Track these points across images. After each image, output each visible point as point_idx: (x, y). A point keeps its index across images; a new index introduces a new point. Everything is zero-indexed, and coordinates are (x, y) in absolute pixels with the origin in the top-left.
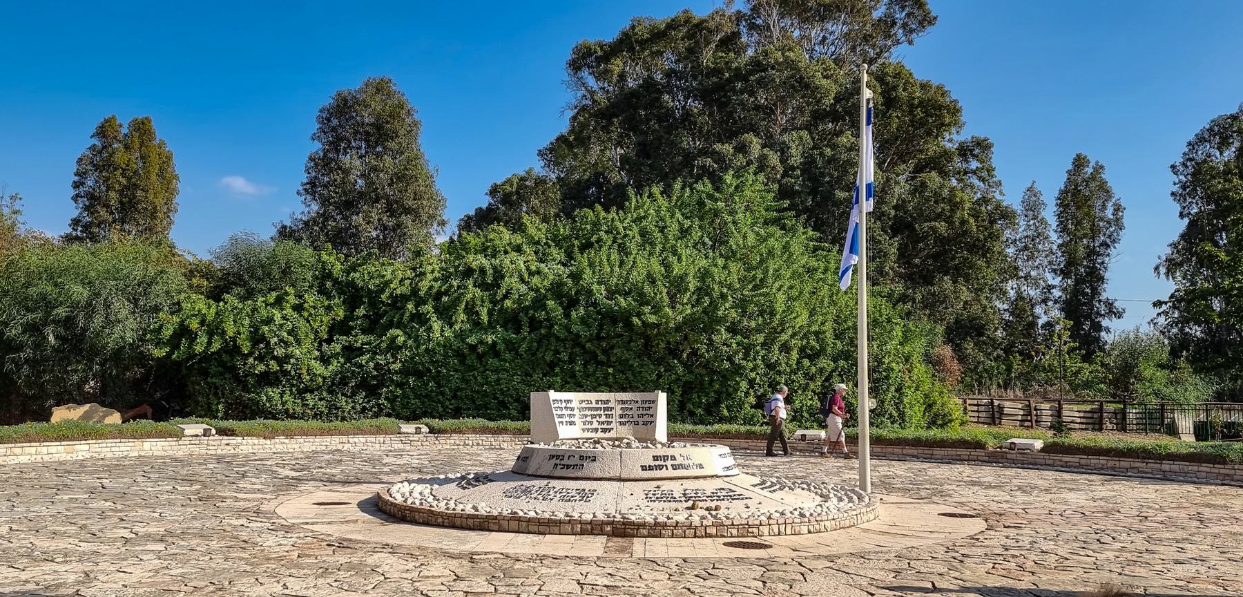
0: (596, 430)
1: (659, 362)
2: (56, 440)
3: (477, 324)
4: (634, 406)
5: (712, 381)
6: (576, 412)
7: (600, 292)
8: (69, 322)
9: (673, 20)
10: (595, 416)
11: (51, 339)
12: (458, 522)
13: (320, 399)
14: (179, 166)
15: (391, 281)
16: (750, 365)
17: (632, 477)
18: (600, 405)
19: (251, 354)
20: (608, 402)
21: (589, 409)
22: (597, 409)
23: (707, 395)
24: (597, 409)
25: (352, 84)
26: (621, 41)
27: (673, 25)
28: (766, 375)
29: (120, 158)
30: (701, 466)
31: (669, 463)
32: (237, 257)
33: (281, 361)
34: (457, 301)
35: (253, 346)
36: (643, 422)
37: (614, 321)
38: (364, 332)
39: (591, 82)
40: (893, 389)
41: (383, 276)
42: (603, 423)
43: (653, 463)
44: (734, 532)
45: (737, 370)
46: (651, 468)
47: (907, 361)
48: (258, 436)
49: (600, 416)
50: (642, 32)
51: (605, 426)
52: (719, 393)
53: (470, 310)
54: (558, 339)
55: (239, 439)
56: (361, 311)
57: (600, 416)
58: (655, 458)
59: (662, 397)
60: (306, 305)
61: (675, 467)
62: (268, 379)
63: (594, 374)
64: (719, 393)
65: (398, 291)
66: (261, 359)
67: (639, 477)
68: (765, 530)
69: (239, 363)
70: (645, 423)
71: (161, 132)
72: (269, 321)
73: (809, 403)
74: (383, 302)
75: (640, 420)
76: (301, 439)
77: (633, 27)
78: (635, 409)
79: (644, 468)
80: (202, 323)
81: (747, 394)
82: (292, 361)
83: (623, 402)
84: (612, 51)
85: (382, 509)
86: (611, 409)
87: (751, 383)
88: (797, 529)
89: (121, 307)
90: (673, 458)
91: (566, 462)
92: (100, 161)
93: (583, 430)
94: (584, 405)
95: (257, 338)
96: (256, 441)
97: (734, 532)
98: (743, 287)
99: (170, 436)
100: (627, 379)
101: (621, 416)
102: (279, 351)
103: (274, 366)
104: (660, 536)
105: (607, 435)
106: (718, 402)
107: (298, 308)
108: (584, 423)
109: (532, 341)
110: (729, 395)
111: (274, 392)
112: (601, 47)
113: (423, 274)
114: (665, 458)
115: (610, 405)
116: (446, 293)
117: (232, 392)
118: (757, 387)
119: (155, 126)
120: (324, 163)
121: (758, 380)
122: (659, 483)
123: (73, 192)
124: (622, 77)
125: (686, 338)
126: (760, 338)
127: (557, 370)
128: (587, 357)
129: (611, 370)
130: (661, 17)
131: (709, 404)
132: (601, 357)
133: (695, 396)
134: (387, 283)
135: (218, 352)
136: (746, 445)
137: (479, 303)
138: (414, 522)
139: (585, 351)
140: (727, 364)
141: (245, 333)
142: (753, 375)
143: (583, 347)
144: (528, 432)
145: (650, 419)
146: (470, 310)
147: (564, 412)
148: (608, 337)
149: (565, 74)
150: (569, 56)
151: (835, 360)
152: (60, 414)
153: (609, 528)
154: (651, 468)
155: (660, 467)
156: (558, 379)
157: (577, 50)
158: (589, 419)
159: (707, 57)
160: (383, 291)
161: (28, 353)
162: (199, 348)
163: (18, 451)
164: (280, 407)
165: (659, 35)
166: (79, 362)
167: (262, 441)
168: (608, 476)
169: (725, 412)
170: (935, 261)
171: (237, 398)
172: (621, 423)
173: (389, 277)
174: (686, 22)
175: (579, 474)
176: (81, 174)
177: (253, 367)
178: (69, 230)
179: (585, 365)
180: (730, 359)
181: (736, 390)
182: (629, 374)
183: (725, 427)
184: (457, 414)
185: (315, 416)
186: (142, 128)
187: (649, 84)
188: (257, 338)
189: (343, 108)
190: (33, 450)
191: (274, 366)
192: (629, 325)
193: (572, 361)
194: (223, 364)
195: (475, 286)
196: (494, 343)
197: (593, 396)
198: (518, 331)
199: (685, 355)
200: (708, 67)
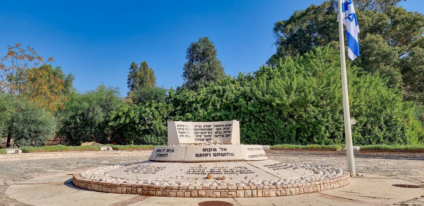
0: (203, 140)
1: (285, 120)
3: (216, 110)
4: (222, 128)
5: (309, 127)
7: (259, 94)
8: (83, 114)
9: (308, 9)
10: (203, 133)
11: (78, 120)
12: (76, 184)
13: (163, 139)
14: (156, 75)
15: (189, 97)
16: (326, 120)
17: (190, 160)
18: (206, 128)
19: (139, 123)
20: (210, 126)
21: (200, 129)
22: (204, 130)
23: (307, 133)
24: (204, 130)
25: (195, 40)
26: (291, 19)
27: (308, 10)
28: (333, 124)
29: (139, 73)
31: (212, 152)
33: (150, 125)
34: (209, 102)
35: (140, 121)
36: (226, 134)
37: (266, 105)
38: (180, 115)
39: (282, 35)
40: (399, 129)
41: (186, 95)
42: (207, 136)
43: (202, 153)
44: (218, 194)
45: (320, 122)
46: (201, 155)
47: (406, 117)
48: (127, 150)
49: (206, 133)
50: (298, 15)
51: (208, 138)
52: (312, 132)
53: (214, 105)
54: (244, 113)
55: (120, 151)
56: (179, 108)
57: (206, 133)
58: (204, 150)
59: (236, 124)
60: (159, 106)
61: (215, 155)
62: (146, 132)
63: (259, 126)
64: (312, 132)
65: (191, 100)
66: (143, 125)
68: (241, 193)
69: (136, 126)
70: (227, 136)
71: (150, 66)
72: (145, 112)
73: (357, 136)
74: (186, 104)
75: (225, 134)
76: (142, 152)
77: (295, 14)
79: (197, 155)
80: (124, 113)
81: (325, 132)
82: (153, 125)
83: (217, 126)
84: (289, 22)
86: (211, 129)
87: (327, 127)
88: (267, 193)
89: (99, 110)
90: (215, 150)
91: (161, 153)
92: (133, 76)
94: (197, 128)
95: (141, 118)
96: (126, 152)
97: (218, 194)
98: (319, 87)
99: (94, 150)
100: (272, 127)
101: (216, 133)
102: (150, 122)
103: (147, 127)
104: (168, 195)
106: (312, 136)
107: (157, 108)
108: (197, 136)
109: (234, 114)
110: (317, 133)
111: (148, 137)
112: (284, 22)
113: (200, 94)
114: (210, 150)
115: (211, 128)
116: (206, 99)
117: (135, 136)
118: (330, 129)
119: (148, 64)
120: (188, 66)
121: (330, 126)
122: (200, 164)
123: (128, 85)
124: (291, 30)
125: (295, 110)
126: (329, 108)
127: (245, 125)
128: (256, 120)
129: (265, 124)
130: (304, 9)
131: (308, 137)
132: (262, 120)
133: (302, 134)
134: (188, 98)
135: (129, 123)
136: (321, 153)
137: (217, 102)
138: (413, 187)
139: (255, 118)
140: (314, 120)
141: (137, 115)
142: (326, 124)
143: (254, 116)
145: (229, 134)
146: (214, 105)
148: (264, 111)
149: (271, 32)
150: (273, 27)
151: (368, 116)
152: (83, 144)
153: (140, 190)
154: (201, 155)
155: (206, 155)
156: (245, 129)
157: (276, 24)
158: (200, 134)
159: (321, 18)
160: (186, 101)
161: (73, 125)
162: (122, 122)
163: (35, 155)
164: (150, 141)
165: (303, 15)
166: (88, 128)
167: (128, 152)
168: (177, 160)
169: (316, 140)
171: (137, 139)
173: (188, 95)
174: (313, 8)
175: (164, 159)
176: (129, 79)
177: (140, 127)
178: (127, 96)
179: (256, 122)
180: (315, 118)
181: (320, 131)
182: (273, 125)
183: (315, 146)
185: (161, 144)
186: (144, 65)
187: (300, 30)
188: (141, 118)
189: (193, 49)
190: (41, 155)
191: (147, 127)
192: (271, 106)
193: (250, 121)
194: (131, 127)
195: (216, 96)
196: (221, 116)
198: (230, 111)
199: (296, 117)
200: (321, 21)
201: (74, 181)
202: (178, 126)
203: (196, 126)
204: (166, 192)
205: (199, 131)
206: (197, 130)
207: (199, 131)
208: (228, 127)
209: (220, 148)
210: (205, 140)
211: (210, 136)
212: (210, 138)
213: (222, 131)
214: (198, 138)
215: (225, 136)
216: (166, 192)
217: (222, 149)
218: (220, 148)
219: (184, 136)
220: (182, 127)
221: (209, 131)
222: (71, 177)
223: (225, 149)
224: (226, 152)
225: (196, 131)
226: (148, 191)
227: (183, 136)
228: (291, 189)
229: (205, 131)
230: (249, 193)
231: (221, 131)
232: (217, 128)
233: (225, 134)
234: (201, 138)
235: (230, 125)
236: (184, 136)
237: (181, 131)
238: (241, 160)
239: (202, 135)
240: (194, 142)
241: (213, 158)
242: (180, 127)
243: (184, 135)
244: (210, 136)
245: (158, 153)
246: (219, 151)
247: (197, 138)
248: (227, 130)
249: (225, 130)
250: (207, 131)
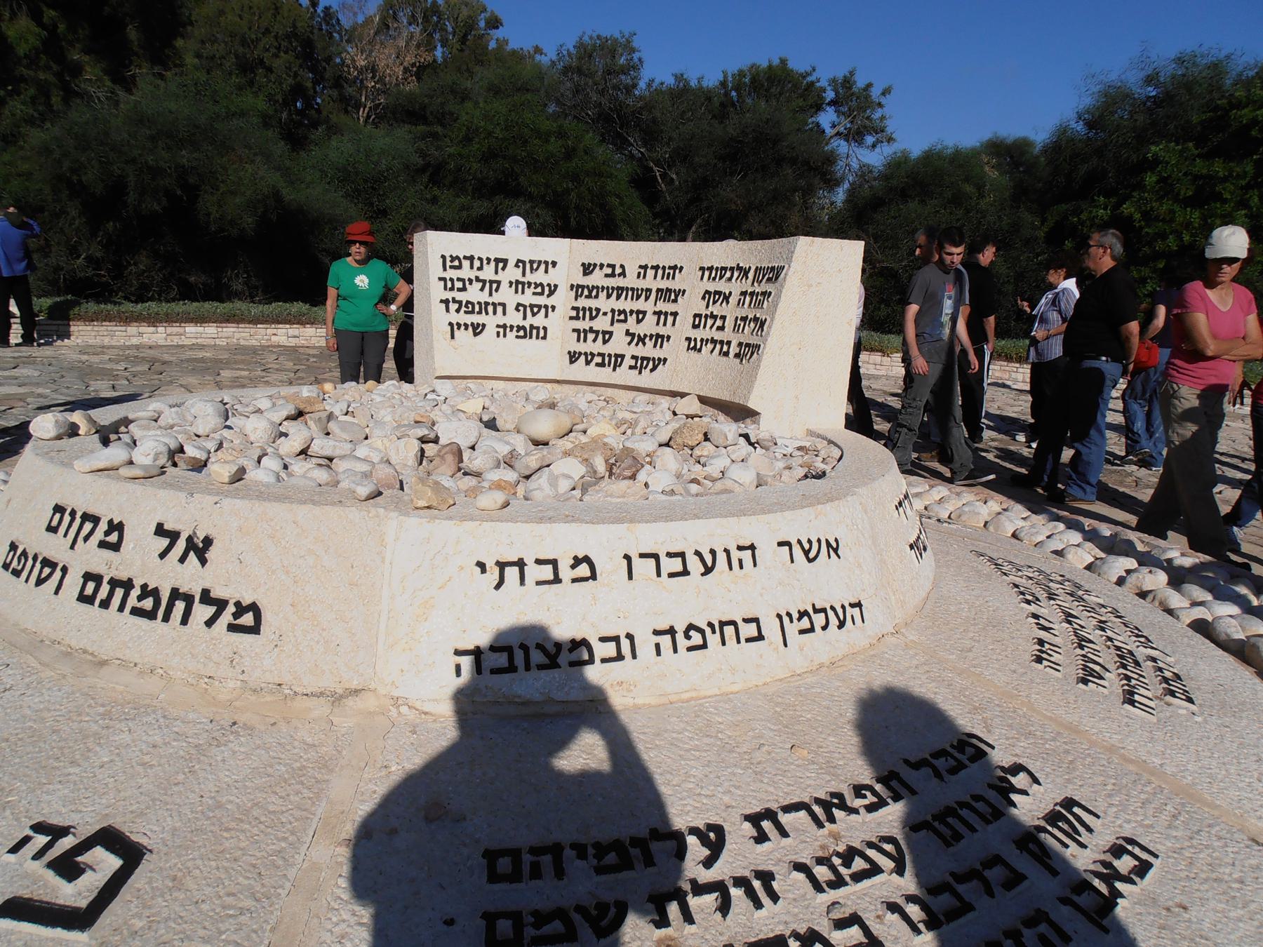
6: (563, 300)
22: (637, 294)
24: (637, 294)
42: (642, 340)
49: (640, 315)
51: (648, 350)
57: (640, 315)
93: (573, 357)
94: (597, 279)
95: (244, 42)
105: (647, 379)
112: (883, 118)
147: (506, 295)
158: (602, 323)
170: (1162, 339)
172: (693, 346)
184: (140, 299)
203: (587, 269)
206: (593, 292)
207: (603, 303)
209: (160, 531)
210: (629, 361)
211: (659, 339)
212: (657, 353)
213: (730, 311)
217: (173, 536)
218: (160, 531)
219: (491, 330)
221: (662, 306)
223: (200, 549)
224: (191, 577)
225: (583, 302)
227: (478, 329)
229: (640, 305)
231: (553, 277)
232: (712, 287)
234: (607, 349)
235: (774, 274)
236: (491, 330)
237: (474, 294)
239: (619, 330)
240: (557, 367)
243: (491, 321)
244: (659, 339)
246: (141, 560)
247: (582, 347)
250: (649, 306)
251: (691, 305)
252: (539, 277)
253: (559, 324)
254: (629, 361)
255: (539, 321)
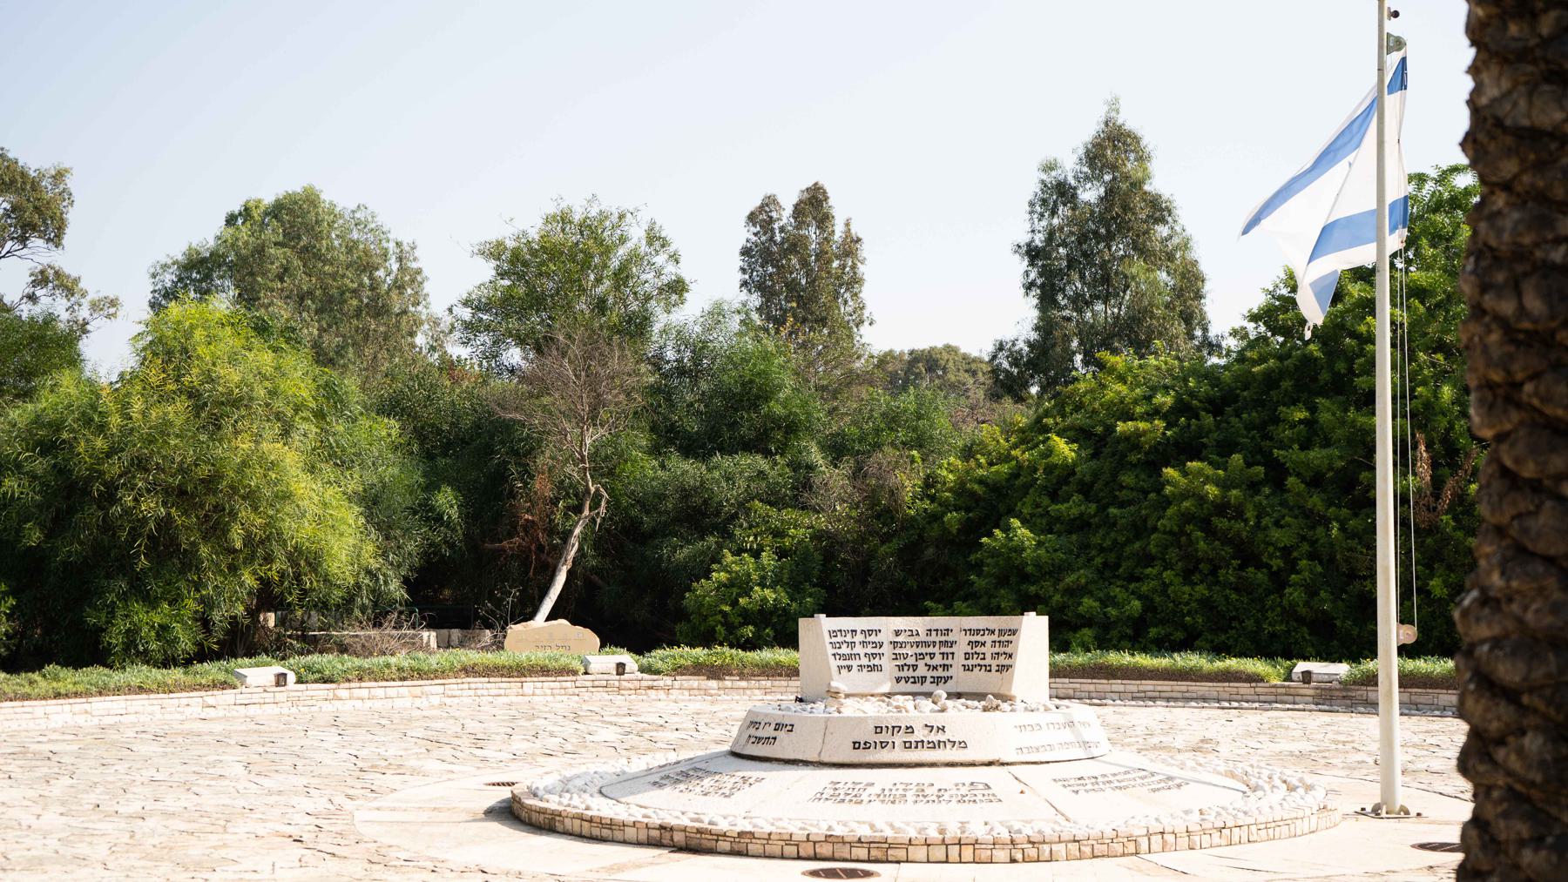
2: (1137, 640)
4: (988, 639)
6: (887, 649)
12: (523, 815)
18: (934, 637)
21: (918, 644)
22: (927, 644)
24: (927, 644)
30: (963, 745)
31: (899, 739)
32: (564, 219)
42: (935, 668)
46: (867, 746)
49: (932, 656)
51: (940, 673)
57: (932, 656)
59: (1034, 628)
61: (907, 746)
67: (847, 760)
75: (994, 663)
78: (988, 645)
79: (856, 745)
85: (1154, 791)
86: (952, 644)
90: (910, 730)
91: (760, 733)
93: (898, 680)
115: (950, 638)
144: (793, 672)
145: (1007, 662)
147: (858, 649)
154: (867, 746)
155: (884, 745)
158: (911, 661)
172: (967, 668)
197: (918, 623)
201: (516, 806)
202: (833, 633)
203: (897, 633)
204: (740, 846)
205: (909, 651)
206: (902, 645)
208: (1006, 638)
210: (929, 680)
212: (945, 674)
214: (905, 673)
215: (994, 668)
216: (740, 846)
219: (855, 669)
220: (849, 638)
221: (944, 650)
222: (505, 793)
225: (898, 651)
226: (696, 843)
227: (849, 668)
228: (1055, 847)
229: (931, 650)
230: (939, 853)
233: (994, 663)
235: (1014, 632)
236: (855, 669)
237: (845, 650)
238: (990, 764)
239: (921, 663)
241: (899, 755)
242: (839, 639)
243: (855, 663)
245: (752, 731)
247: (902, 674)
248: (1002, 650)
249: (997, 650)
250: (936, 650)
251: (961, 648)
252: (873, 638)
253: (887, 663)
254: (929, 680)
255: (876, 661)
